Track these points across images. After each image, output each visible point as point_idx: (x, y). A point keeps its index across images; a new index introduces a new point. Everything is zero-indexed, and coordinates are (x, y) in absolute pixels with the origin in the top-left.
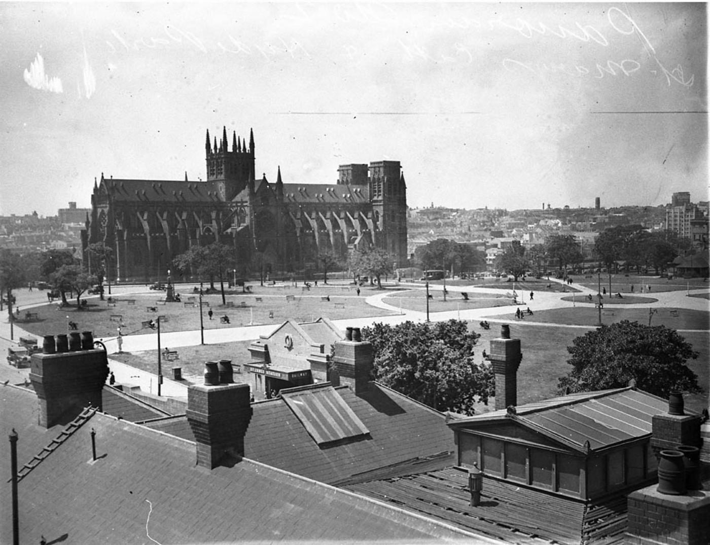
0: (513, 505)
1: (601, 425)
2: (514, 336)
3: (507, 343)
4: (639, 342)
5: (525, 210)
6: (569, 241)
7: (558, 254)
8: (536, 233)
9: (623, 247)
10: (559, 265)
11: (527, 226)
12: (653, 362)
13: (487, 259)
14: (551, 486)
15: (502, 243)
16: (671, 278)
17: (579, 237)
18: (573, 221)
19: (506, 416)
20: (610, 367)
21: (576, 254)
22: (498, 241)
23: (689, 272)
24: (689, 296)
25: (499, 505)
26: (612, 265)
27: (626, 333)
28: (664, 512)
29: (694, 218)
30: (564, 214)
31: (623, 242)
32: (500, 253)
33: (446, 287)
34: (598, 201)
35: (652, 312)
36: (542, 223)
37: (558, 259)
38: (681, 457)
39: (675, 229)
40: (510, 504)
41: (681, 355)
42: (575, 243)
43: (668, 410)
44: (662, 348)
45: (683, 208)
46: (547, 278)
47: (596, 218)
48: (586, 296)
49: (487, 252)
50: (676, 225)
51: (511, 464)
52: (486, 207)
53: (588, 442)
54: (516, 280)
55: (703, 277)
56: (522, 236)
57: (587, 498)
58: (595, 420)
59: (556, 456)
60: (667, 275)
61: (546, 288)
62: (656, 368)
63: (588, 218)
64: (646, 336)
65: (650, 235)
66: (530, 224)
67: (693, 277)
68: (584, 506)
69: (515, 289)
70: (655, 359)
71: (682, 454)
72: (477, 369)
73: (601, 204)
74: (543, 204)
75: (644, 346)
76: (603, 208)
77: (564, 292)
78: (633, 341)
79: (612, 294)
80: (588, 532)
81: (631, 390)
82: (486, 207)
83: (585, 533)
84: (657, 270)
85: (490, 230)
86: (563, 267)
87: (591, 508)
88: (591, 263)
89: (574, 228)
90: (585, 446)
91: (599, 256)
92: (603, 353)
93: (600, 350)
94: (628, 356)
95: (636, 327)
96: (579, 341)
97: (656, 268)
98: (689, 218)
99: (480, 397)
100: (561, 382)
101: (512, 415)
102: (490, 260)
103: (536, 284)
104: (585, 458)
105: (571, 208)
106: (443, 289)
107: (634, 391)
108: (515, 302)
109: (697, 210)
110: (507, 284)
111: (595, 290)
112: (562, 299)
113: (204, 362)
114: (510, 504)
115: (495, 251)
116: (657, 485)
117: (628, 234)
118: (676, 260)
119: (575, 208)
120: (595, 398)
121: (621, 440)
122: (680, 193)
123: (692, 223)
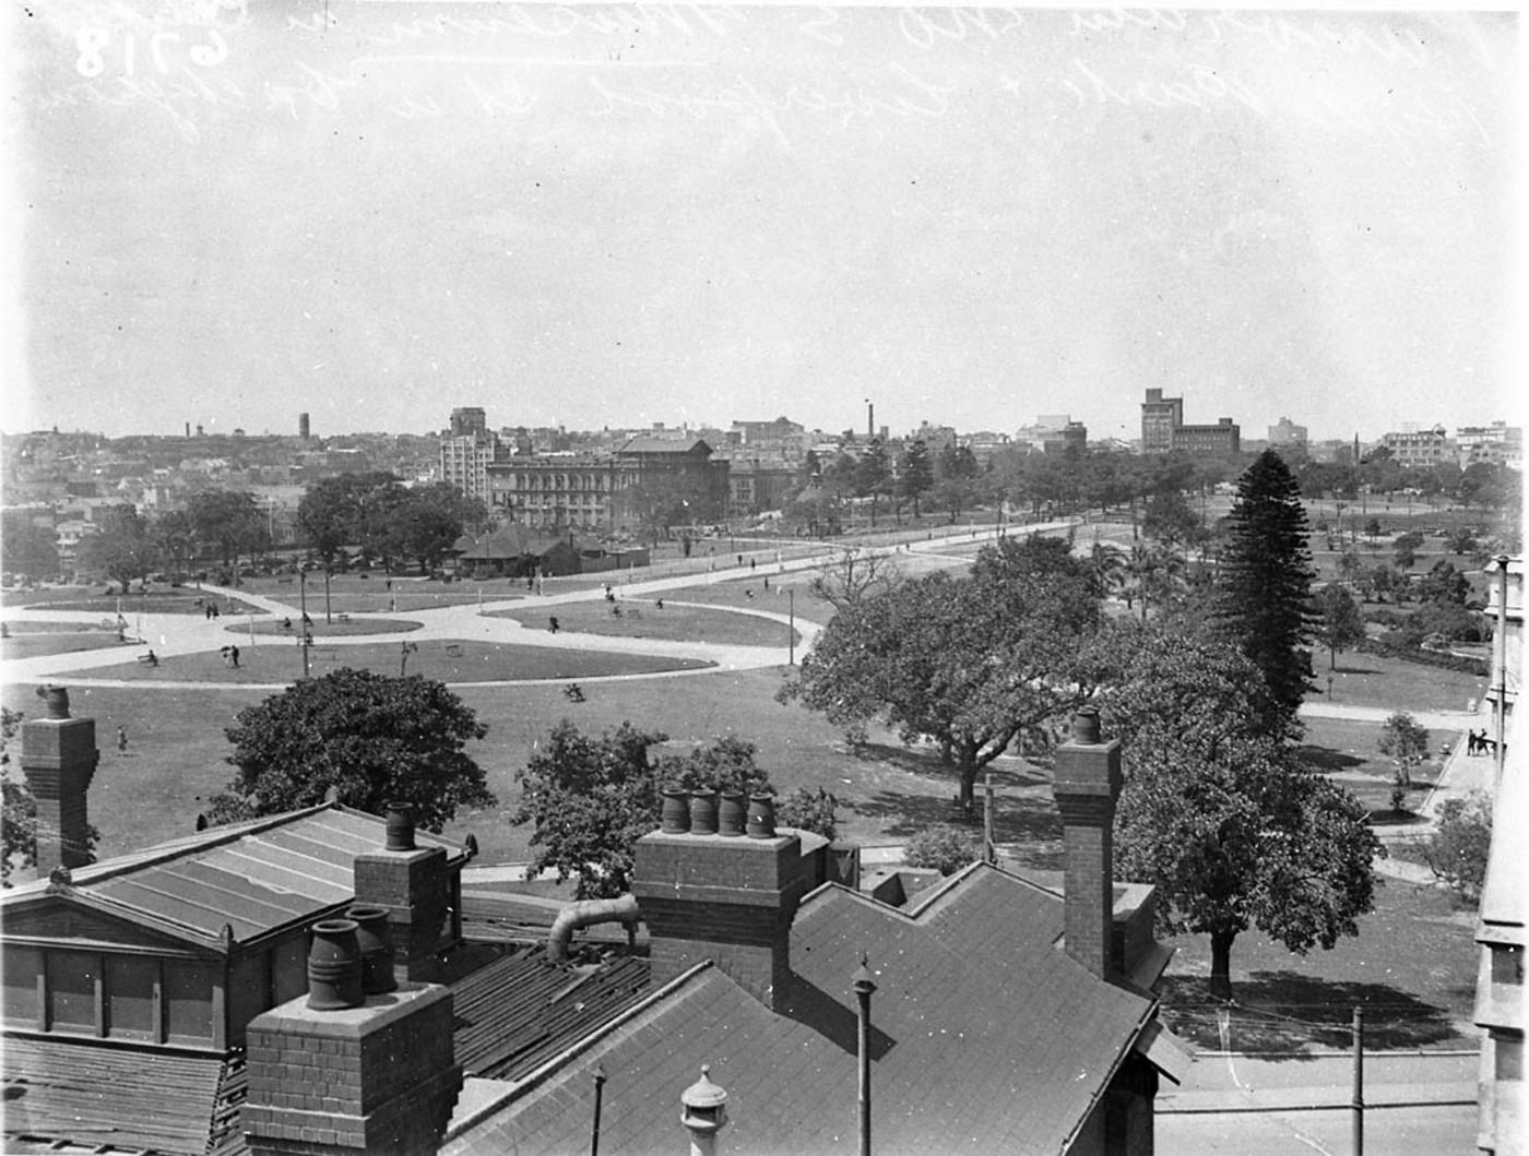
0: (63, 1088)
1: (265, 890)
2: (76, 714)
3: (63, 728)
4: (373, 710)
5: (146, 437)
6: (242, 504)
7: (218, 533)
8: (172, 488)
9: (355, 519)
10: (222, 556)
11: (151, 472)
12: (400, 751)
13: (60, 546)
14: (152, 1034)
15: (95, 509)
16: (448, 579)
17: (266, 497)
18: (255, 463)
19: (48, 891)
20: (314, 766)
21: (258, 533)
22: (86, 504)
23: (483, 567)
24: (483, 614)
25: (29, 1094)
26: (335, 555)
27: (348, 694)
28: (317, 1048)
29: (492, 460)
30: (236, 446)
31: (355, 507)
32: (89, 531)
33: (788, 622)
34: (305, 420)
35: (409, 648)
36: (185, 465)
37: (220, 543)
38: (352, 932)
39: (459, 481)
40: (55, 1087)
41: (454, 733)
42: (258, 511)
43: (385, 841)
44: (418, 720)
45: (471, 440)
46: (194, 586)
47: (303, 457)
48: (279, 622)
49: (59, 529)
50: (459, 473)
51: (63, 999)
52: (56, 428)
53: (230, 927)
54: (125, 591)
55: (508, 576)
56: (140, 495)
57: (227, 1048)
58: (251, 880)
59: (162, 963)
60: (442, 574)
61: (193, 608)
62: (407, 762)
63: (286, 457)
64: (386, 698)
65: (408, 493)
66: (157, 467)
67: (491, 577)
68: (220, 1063)
69: (121, 610)
70: (404, 745)
71: (355, 924)
72: (17, 792)
73: (311, 427)
74: (188, 425)
75: (381, 719)
76: (316, 437)
77: (232, 613)
78: (361, 710)
79: (333, 616)
80: (226, 1119)
81: (330, 810)
82: (56, 428)
83: (219, 1121)
84: (423, 565)
85: (65, 480)
86: (231, 562)
87: (236, 1066)
88: (293, 552)
89: (256, 478)
90: (222, 936)
91: (307, 536)
92: (301, 737)
93: (294, 732)
94: (352, 739)
95: (367, 680)
96: (250, 716)
97: (422, 561)
98: (484, 460)
99: (25, 857)
100: (214, 806)
101: (63, 886)
102: (67, 547)
103: (171, 598)
104: (224, 963)
105: (249, 434)
106: (301, 616)
107: (335, 812)
108: (122, 638)
109: (498, 444)
110: (107, 600)
111: (294, 606)
112: (226, 629)
113: (1358, 942)
114: (55, 1087)
115: (79, 527)
116: (308, 996)
117: (365, 491)
118: (458, 545)
119: (258, 434)
120: (253, 832)
121: (300, 915)
122: (466, 410)
123: (488, 470)
